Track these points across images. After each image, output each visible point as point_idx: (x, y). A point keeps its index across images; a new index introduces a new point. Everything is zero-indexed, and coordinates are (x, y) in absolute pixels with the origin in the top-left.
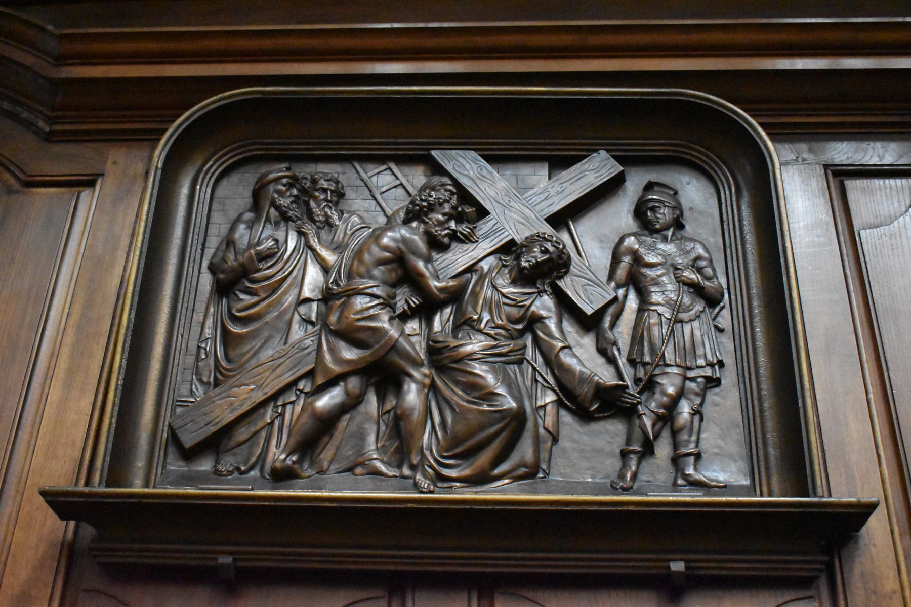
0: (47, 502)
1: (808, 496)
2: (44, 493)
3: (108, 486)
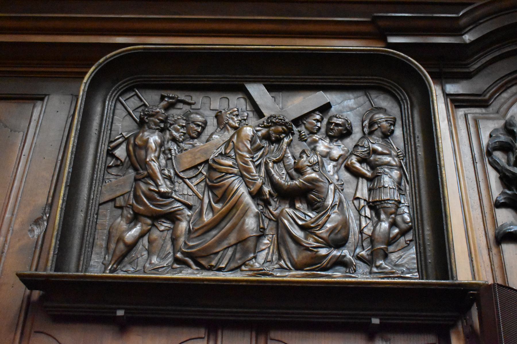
0: (21, 280)
1: (448, 279)
2: (17, 275)
3: (55, 271)
